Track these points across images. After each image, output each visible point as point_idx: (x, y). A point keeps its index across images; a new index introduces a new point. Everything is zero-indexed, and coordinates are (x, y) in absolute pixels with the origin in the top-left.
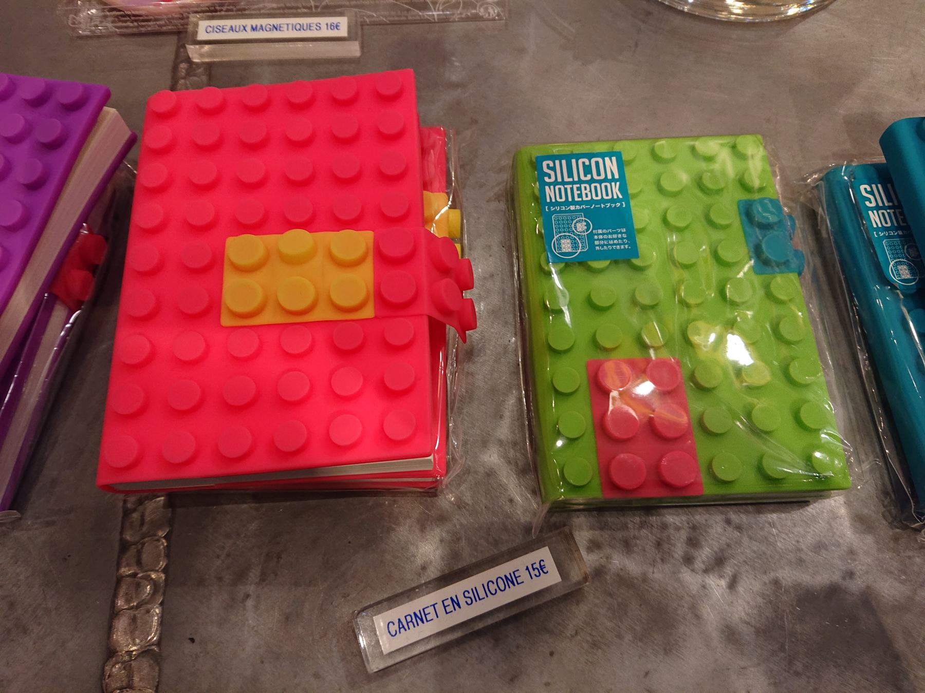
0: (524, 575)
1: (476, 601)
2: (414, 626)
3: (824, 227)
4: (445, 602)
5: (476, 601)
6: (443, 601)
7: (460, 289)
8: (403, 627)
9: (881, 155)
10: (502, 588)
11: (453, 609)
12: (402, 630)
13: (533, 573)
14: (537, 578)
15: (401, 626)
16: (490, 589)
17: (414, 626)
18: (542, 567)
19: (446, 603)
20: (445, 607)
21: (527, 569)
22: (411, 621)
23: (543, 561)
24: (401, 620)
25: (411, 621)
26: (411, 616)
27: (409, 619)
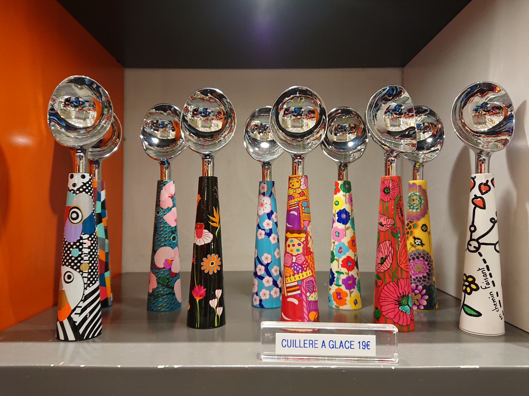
0: (356, 345)
1: (293, 347)
2: (313, 347)
3: (198, 282)
4: (305, 341)
5: (293, 347)
6: (304, 340)
7: (82, 231)
8: (342, 346)
9: (225, 272)
10: (289, 346)
11: (308, 346)
12: (341, 347)
13: (361, 346)
14: (362, 349)
15: (323, 345)
16: (283, 344)
17: (313, 347)
18: (368, 345)
19: (306, 342)
20: (304, 344)
21: (359, 343)
22: (312, 344)
23: (370, 342)
24: (343, 342)
25: (312, 344)
26: (313, 341)
27: (311, 342)
